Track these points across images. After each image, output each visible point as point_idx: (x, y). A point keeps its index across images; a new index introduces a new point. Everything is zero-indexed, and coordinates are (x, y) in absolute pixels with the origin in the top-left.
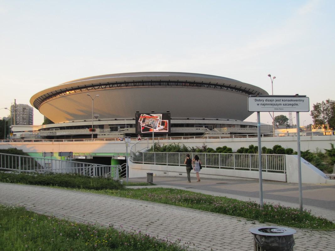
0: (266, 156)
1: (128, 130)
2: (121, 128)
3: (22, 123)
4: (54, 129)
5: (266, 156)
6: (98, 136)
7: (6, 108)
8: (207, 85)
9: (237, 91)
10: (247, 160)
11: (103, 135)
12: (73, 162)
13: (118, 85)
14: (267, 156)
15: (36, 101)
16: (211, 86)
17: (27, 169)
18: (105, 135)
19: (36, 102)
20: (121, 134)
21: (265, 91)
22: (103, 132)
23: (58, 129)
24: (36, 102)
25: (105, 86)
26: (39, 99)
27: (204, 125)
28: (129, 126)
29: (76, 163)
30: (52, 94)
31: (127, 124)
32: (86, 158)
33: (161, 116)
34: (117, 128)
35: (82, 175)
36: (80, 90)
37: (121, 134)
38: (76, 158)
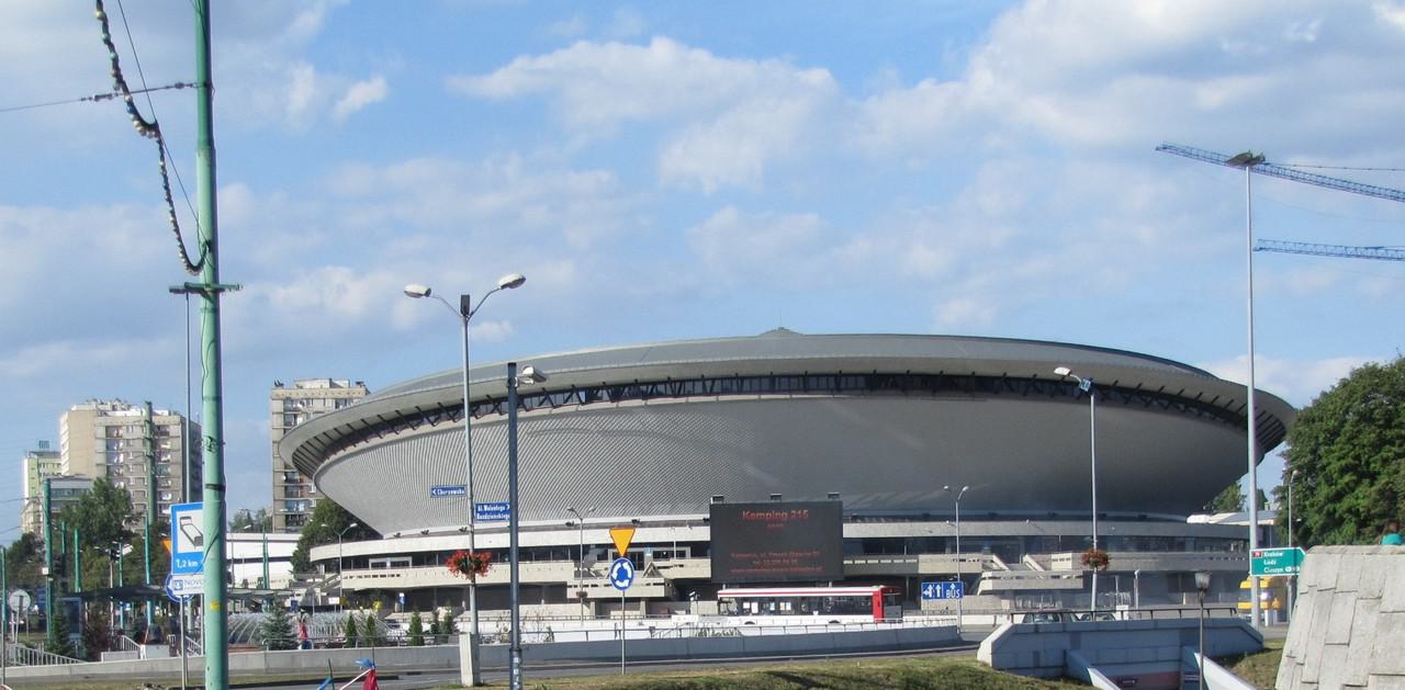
1: (682, 566)
2: (657, 556)
4: (388, 562)
6: (569, 590)
7: (1247, 161)
8: (567, 395)
11: (393, 576)
15: (302, 450)
18: (596, 586)
19: (300, 455)
20: (655, 584)
21: (1279, 399)
22: (587, 575)
23: (405, 559)
24: (300, 455)
26: (316, 443)
27: (986, 543)
28: (688, 550)
30: (351, 430)
31: (679, 544)
36: (559, 639)
37: (655, 584)
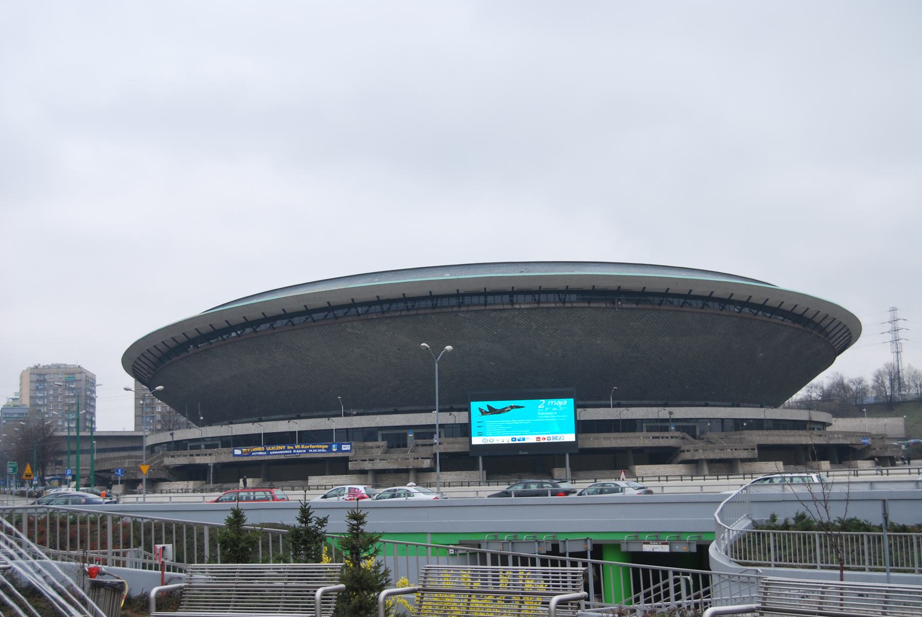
0: (771, 535)
3: (63, 422)
5: (771, 535)
8: (682, 301)
9: (769, 315)
10: (907, 553)
12: (621, 566)
13: (409, 304)
14: (889, 536)
16: (693, 302)
17: (206, 559)
25: (365, 309)
26: (148, 355)
29: (628, 567)
32: (670, 548)
33: (484, 405)
34: (405, 436)
35: (342, 580)
36: (268, 325)
38: (634, 548)
